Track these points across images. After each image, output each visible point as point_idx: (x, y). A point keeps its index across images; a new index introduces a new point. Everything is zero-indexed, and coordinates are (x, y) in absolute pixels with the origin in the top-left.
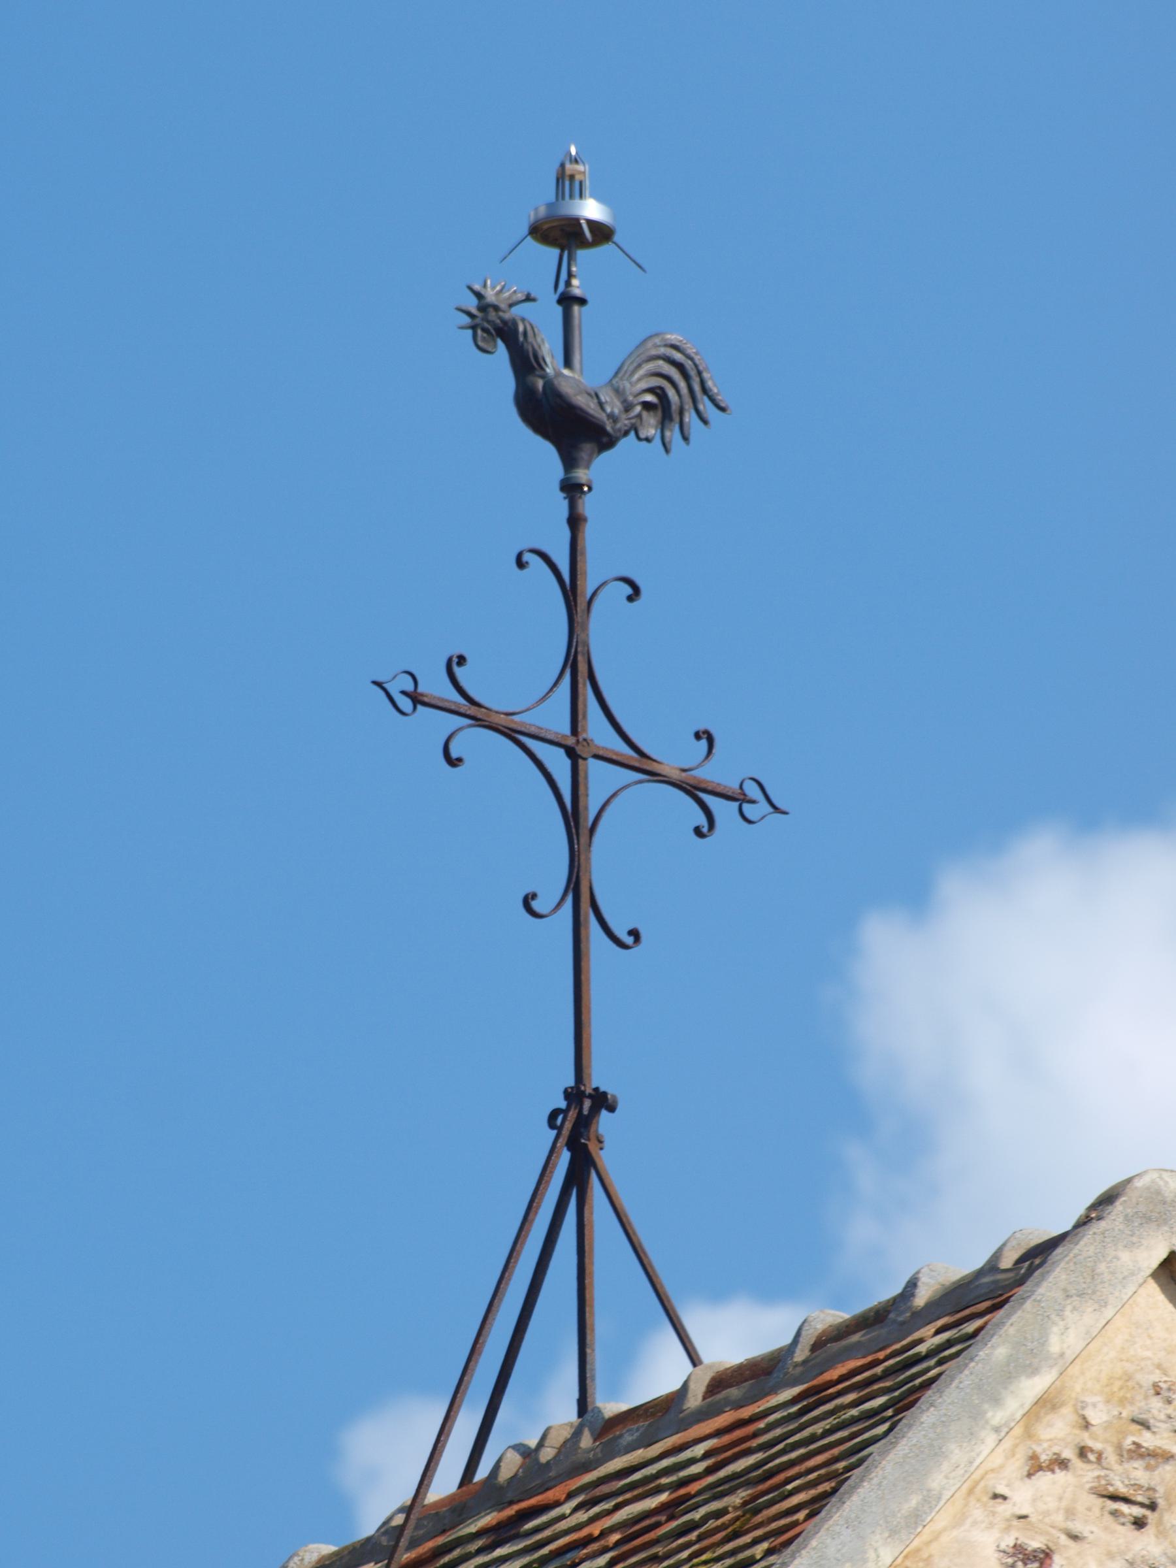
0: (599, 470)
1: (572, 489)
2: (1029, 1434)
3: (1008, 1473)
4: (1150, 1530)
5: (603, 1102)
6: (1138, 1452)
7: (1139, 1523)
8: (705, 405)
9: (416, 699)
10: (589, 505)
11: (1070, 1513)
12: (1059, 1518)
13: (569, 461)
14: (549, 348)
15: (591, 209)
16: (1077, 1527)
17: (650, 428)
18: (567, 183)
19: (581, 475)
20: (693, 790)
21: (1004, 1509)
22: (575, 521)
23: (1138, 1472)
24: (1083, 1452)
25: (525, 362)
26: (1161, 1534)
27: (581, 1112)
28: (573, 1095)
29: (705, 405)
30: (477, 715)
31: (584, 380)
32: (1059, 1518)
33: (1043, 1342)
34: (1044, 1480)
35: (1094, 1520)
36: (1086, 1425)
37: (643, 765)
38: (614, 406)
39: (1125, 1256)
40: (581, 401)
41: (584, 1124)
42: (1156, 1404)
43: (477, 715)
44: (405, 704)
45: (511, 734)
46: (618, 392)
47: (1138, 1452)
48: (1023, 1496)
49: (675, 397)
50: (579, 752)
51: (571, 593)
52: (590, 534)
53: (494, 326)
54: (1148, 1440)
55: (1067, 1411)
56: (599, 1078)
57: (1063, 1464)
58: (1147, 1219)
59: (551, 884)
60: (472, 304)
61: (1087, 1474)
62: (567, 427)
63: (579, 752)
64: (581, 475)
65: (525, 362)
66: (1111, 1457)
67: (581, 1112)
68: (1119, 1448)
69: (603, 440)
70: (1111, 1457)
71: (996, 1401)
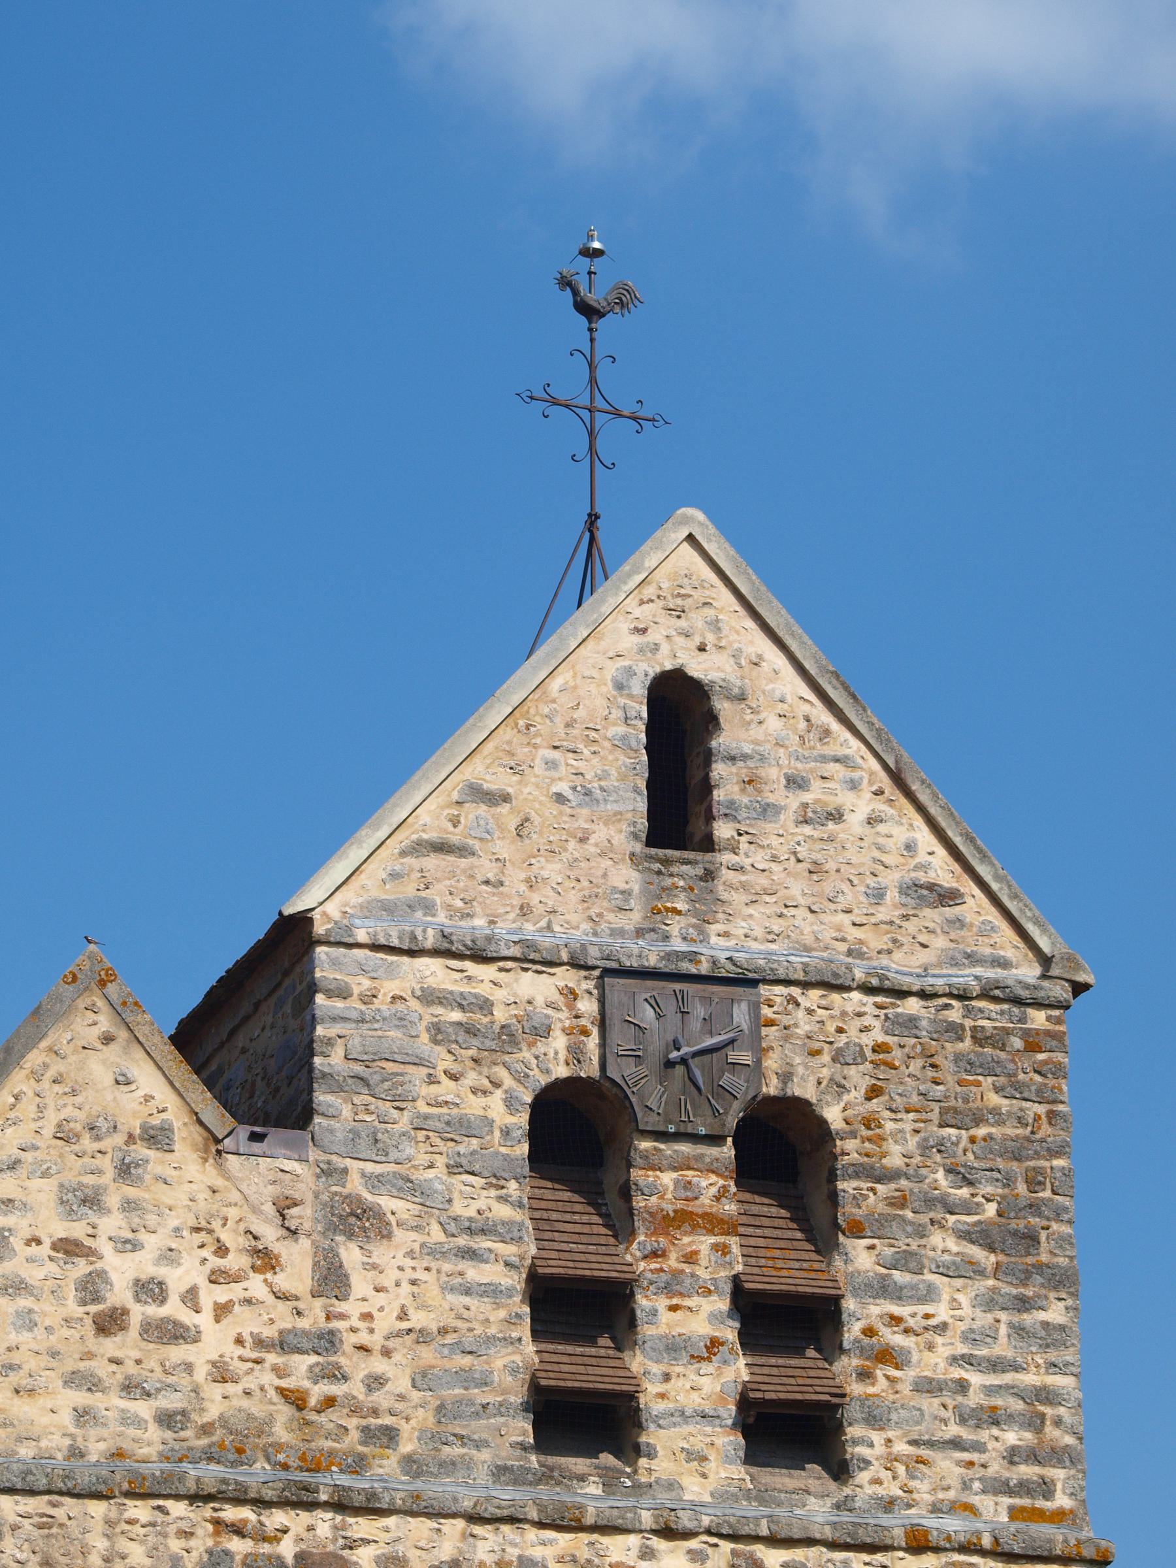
0: (601, 324)
1: (590, 330)
2: (640, 593)
3: (632, 603)
4: (683, 619)
5: (597, 517)
6: (679, 595)
7: (679, 617)
8: (637, 303)
9: (532, 398)
10: (596, 335)
11: (654, 616)
12: (650, 618)
13: (590, 323)
14: (583, 289)
15: (596, 245)
16: (656, 620)
17: (617, 309)
18: (591, 238)
19: (593, 325)
20: (635, 419)
21: (631, 616)
22: (592, 340)
23: (679, 601)
24: (659, 597)
25: (575, 293)
26: (687, 619)
27: (593, 518)
28: (590, 515)
29: (637, 303)
30: (555, 402)
31: (594, 297)
32: (650, 618)
33: (643, 564)
34: (645, 606)
35: (663, 618)
36: (661, 588)
37: (618, 414)
38: (605, 304)
39: (673, 536)
40: (592, 303)
41: (592, 523)
42: (686, 580)
43: (555, 402)
44: (529, 400)
45: (567, 406)
46: (606, 299)
47: (679, 595)
48: (637, 612)
49: (623, 300)
50: (593, 411)
51: (591, 365)
52: (597, 344)
53: (566, 283)
54: (682, 591)
55: (654, 585)
56: (597, 510)
57: (652, 601)
58: (681, 523)
59: (582, 449)
60: (559, 276)
61: (661, 603)
62: (588, 311)
63: (593, 411)
64: (593, 325)
65: (575, 293)
66: (669, 597)
67: (593, 518)
68: (672, 594)
69: (602, 315)
70: (669, 597)
71: (625, 583)
